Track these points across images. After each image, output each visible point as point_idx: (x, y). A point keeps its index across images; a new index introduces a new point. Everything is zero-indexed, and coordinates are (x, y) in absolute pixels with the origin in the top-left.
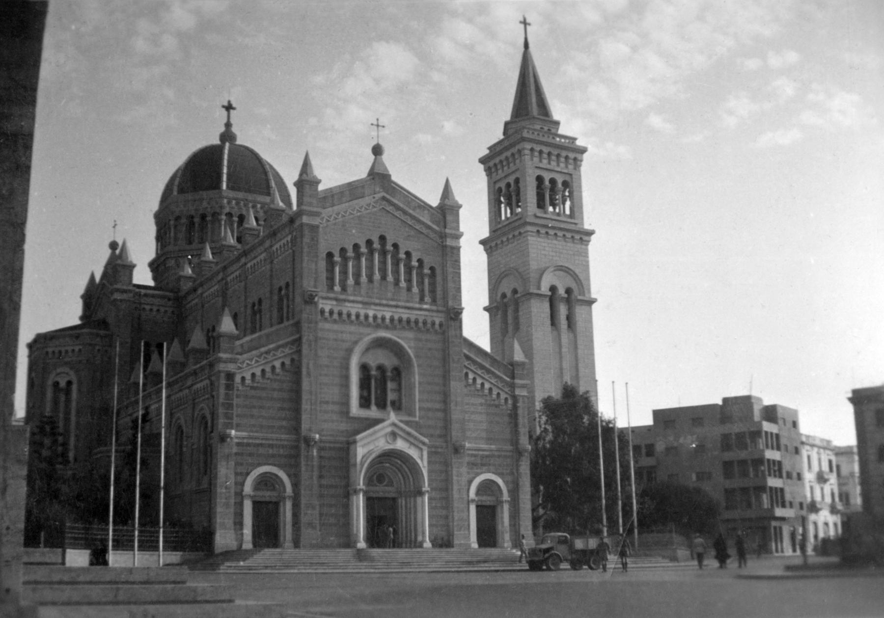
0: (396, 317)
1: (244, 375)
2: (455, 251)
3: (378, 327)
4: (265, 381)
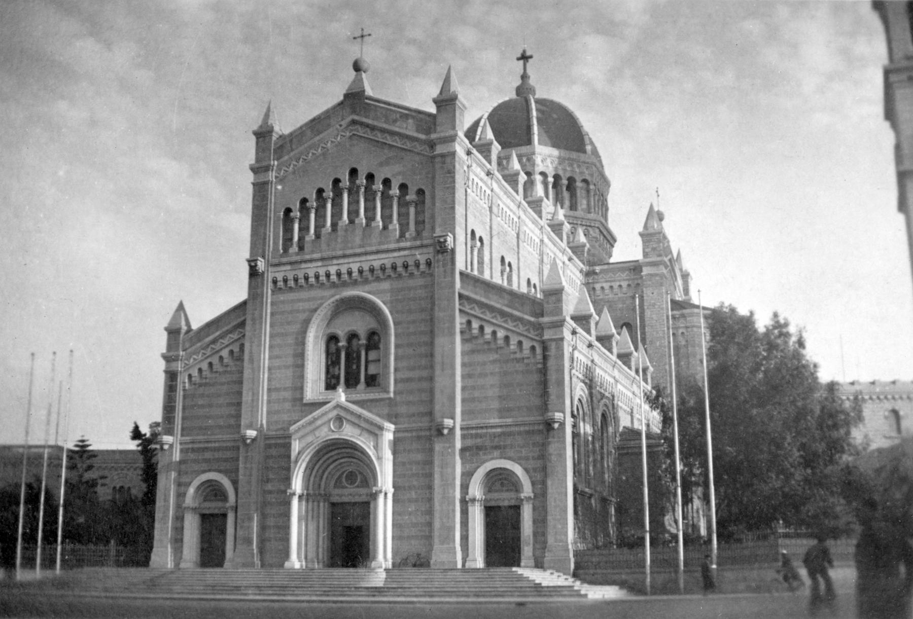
0: (366, 267)
2: (448, 160)
3: (344, 284)
4: (214, 375)
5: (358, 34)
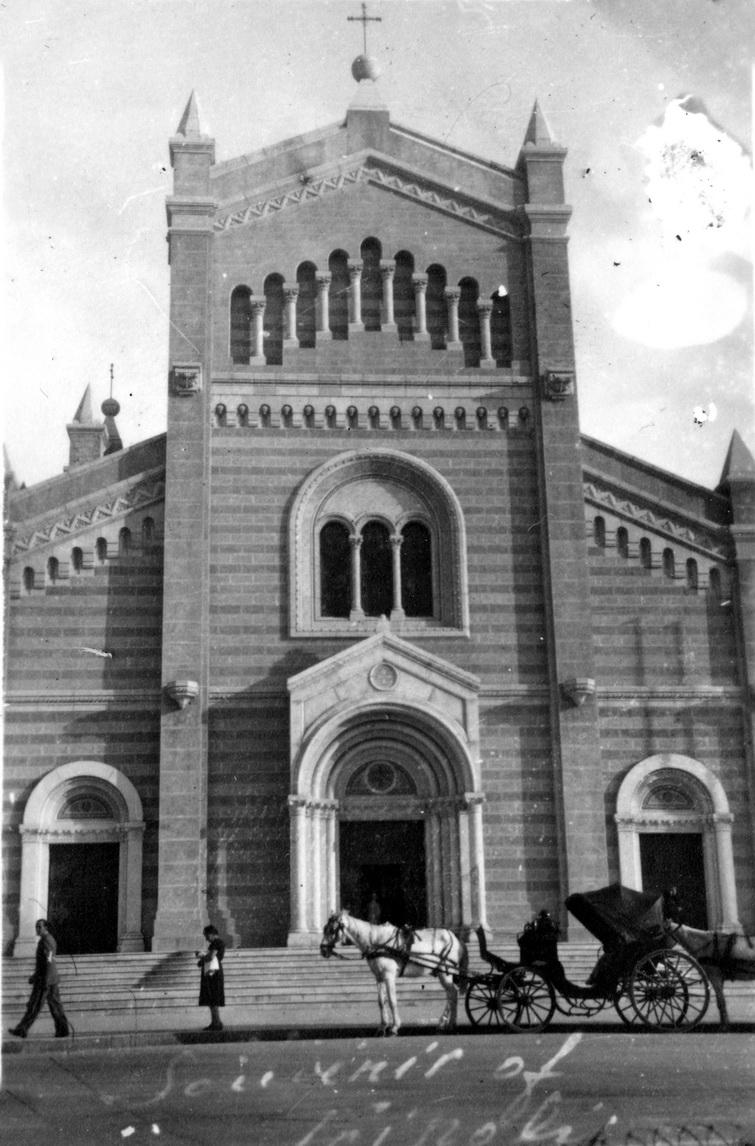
1: (32, 564)
5: (359, 13)
